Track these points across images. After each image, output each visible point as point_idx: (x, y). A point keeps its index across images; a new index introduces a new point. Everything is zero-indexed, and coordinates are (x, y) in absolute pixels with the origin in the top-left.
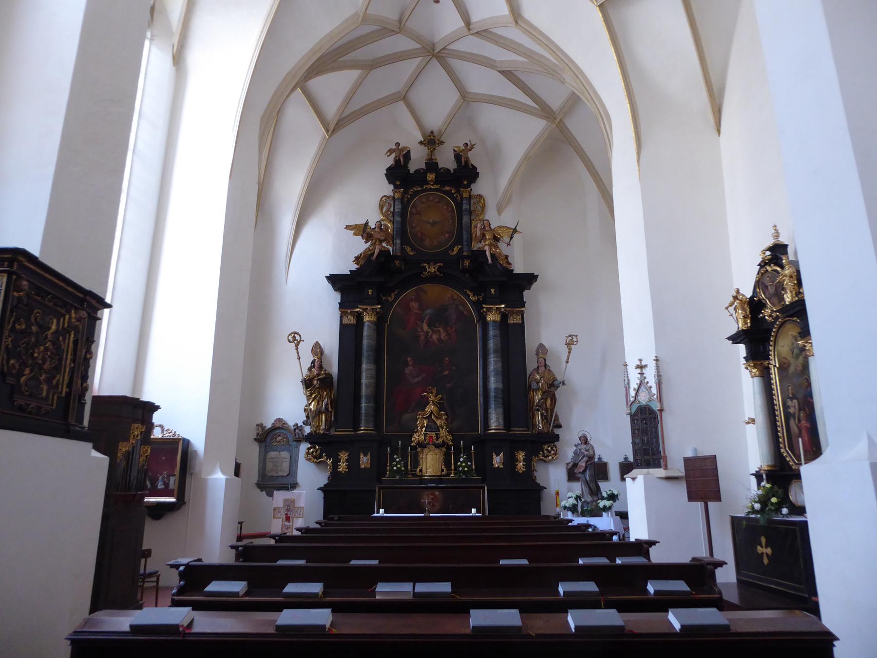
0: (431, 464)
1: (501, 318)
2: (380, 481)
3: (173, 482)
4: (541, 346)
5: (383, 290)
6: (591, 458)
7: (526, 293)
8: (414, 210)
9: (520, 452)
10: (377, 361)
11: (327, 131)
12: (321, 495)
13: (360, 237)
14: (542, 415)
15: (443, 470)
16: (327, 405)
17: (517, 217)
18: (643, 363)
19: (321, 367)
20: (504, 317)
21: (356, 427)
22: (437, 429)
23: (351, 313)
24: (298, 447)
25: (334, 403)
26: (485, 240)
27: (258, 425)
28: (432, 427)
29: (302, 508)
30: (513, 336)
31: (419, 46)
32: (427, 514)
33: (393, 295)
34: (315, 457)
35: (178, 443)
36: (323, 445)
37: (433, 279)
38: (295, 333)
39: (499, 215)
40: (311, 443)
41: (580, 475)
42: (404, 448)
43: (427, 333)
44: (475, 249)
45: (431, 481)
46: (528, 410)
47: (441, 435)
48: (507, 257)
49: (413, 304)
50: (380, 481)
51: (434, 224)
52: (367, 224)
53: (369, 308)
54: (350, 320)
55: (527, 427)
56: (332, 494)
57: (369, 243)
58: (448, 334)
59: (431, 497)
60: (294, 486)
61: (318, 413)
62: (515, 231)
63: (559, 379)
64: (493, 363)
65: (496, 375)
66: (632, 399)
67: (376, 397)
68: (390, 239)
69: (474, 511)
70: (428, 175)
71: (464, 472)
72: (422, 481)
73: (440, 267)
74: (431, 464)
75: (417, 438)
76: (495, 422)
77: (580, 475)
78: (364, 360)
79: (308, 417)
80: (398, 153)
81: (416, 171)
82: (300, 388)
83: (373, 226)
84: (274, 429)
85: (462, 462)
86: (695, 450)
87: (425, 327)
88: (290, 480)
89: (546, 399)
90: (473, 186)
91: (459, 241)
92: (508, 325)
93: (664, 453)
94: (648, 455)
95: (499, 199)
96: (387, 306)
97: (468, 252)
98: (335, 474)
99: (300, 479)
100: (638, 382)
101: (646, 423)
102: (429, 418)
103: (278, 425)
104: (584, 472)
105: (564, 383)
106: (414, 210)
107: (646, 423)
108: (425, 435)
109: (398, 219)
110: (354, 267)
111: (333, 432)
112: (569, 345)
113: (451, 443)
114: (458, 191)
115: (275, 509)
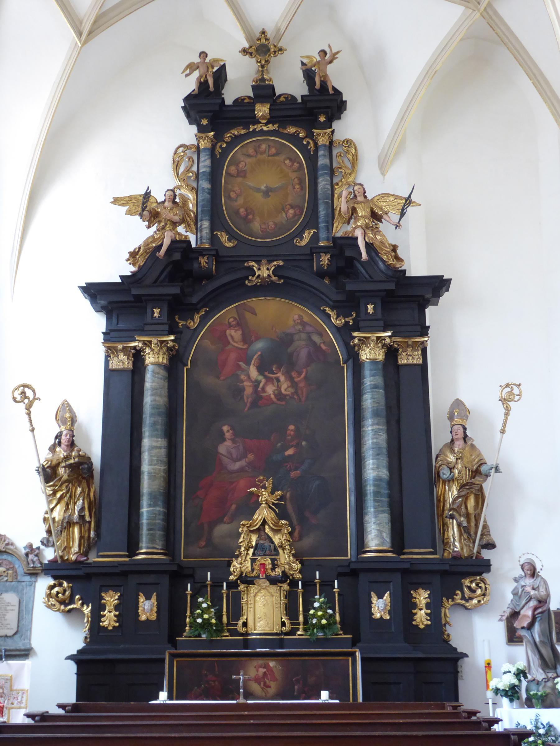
0: (263, 611)
1: (387, 355)
2: (173, 643)
4: (458, 403)
5: (178, 308)
6: (543, 602)
7: (430, 311)
11: (79, 34)
12: (72, 667)
13: (138, 218)
14: (459, 525)
15: (283, 624)
16: (82, 509)
19: (72, 445)
20: (392, 353)
21: (132, 547)
22: (274, 552)
23: (124, 349)
24: (32, 585)
25: (96, 506)
26: (357, 219)
28: (264, 548)
29: (24, 691)
30: (407, 388)
32: (242, 700)
33: (197, 317)
34: (62, 602)
36: (77, 580)
37: (266, 289)
38: (25, 386)
39: (383, 174)
40: (55, 577)
41: (523, 633)
42: (216, 585)
43: (258, 382)
44: (339, 235)
45: (264, 643)
46: (434, 514)
47: (283, 561)
48: (394, 248)
49: (233, 332)
50: (173, 643)
51: (267, 193)
52: (147, 195)
53: (154, 340)
54: (122, 362)
55: (434, 546)
56: (90, 666)
57: (154, 228)
58: (294, 384)
59: (262, 670)
60: (25, 653)
61: (68, 524)
62: (408, 201)
64: (374, 434)
65: (377, 455)
67: (169, 496)
68: (194, 223)
69: (325, 695)
70: (258, 107)
71: (322, 628)
72: (246, 644)
73: (278, 267)
74: (263, 611)
75: (237, 567)
76: (376, 536)
77: (523, 633)
78: (146, 431)
79: (49, 532)
80: (203, 69)
81: (236, 101)
82: (37, 481)
83: (160, 199)
85: (316, 609)
87: (254, 373)
88: (20, 644)
89: (466, 498)
90: (336, 125)
91: (311, 220)
92: (398, 367)
96: (184, 338)
97: (328, 240)
98: (96, 631)
99: (35, 643)
102: (260, 530)
104: (530, 627)
105: (497, 470)
106: (233, 170)
108: (253, 561)
109: (205, 185)
110: (128, 269)
111: (93, 558)
112: (505, 401)
113: (298, 576)
114: (310, 135)
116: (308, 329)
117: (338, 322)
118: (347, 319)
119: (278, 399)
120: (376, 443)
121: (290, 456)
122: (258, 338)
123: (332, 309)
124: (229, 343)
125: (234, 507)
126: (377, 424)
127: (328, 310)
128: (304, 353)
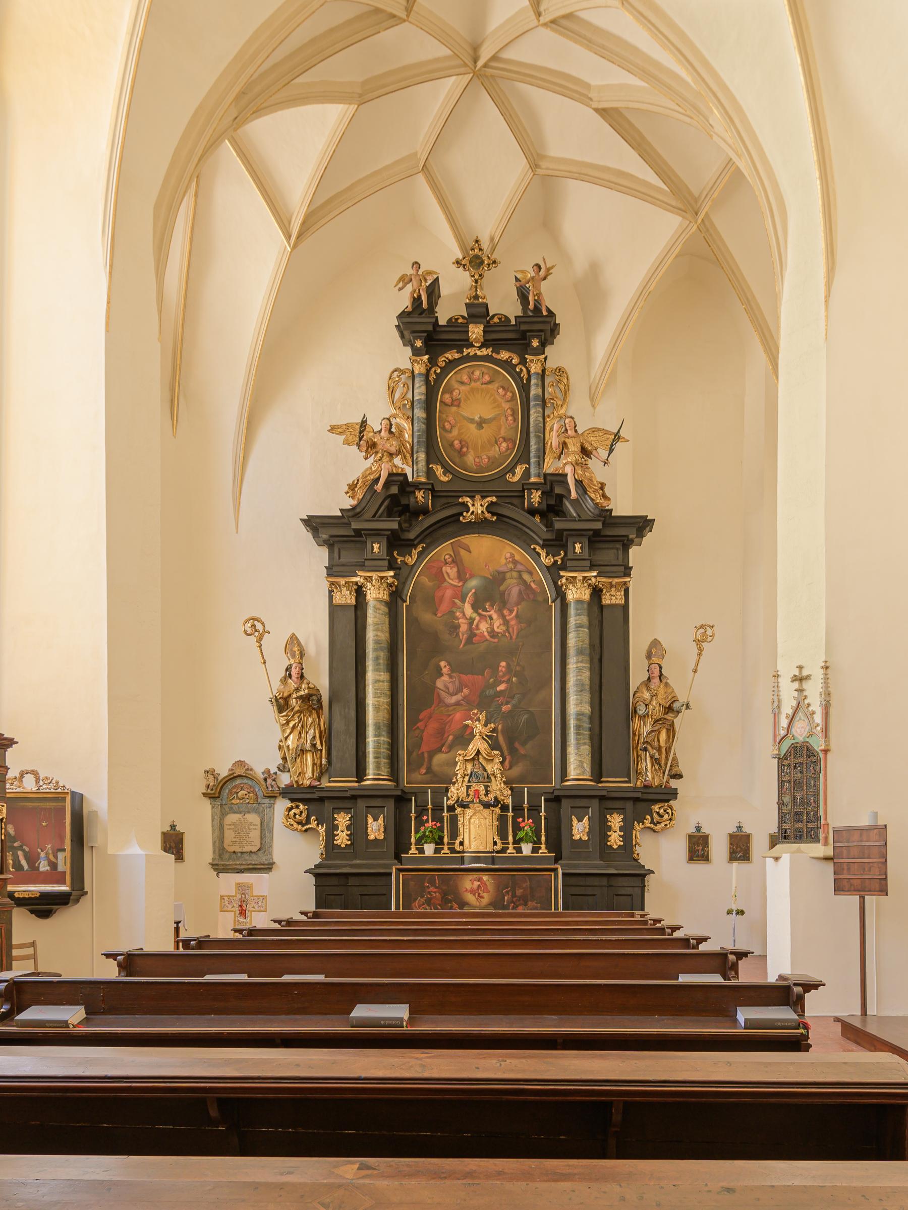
0: (477, 832)
1: (592, 594)
3: (64, 862)
4: (655, 643)
5: (397, 543)
7: (633, 551)
8: (447, 397)
9: (615, 816)
10: (393, 667)
11: (288, 237)
12: (312, 879)
14: (652, 757)
15: (495, 843)
17: (614, 411)
18: (805, 673)
20: (597, 593)
24: (271, 807)
25: (327, 736)
27: (207, 772)
30: (608, 627)
31: (446, 52)
33: (415, 553)
34: (300, 823)
35: (64, 799)
36: (313, 802)
37: (480, 526)
38: (254, 619)
40: (292, 800)
48: (602, 486)
50: (398, 858)
51: (481, 424)
52: (364, 424)
53: (375, 575)
55: (629, 776)
57: (371, 460)
58: (506, 623)
59: (477, 883)
62: (617, 437)
63: (682, 699)
65: (580, 691)
66: (783, 733)
70: (471, 327)
74: (477, 832)
75: (456, 791)
76: (578, 767)
81: (450, 320)
84: (232, 778)
86: (875, 815)
87: (468, 610)
90: (548, 350)
91: (523, 456)
92: (601, 607)
93: (826, 819)
94: (800, 821)
95: (597, 378)
98: (330, 847)
99: (277, 856)
100: (794, 703)
101: (801, 769)
103: (239, 772)
106: (447, 397)
107: (801, 769)
108: (468, 787)
109: (420, 413)
110: (349, 503)
111: (325, 783)
114: (523, 362)
115: (222, 897)
116: (519, 567)
117: (547, 561)
118: (556, 558)
119: (491, 637)
120: (580, 680)
121: (501, 691)
122: (472, 576)
123: (542, 547)
124: (445, 580)
125: (451, 738)
126: (581, 662)
127: (538, 549)
128: (515, 591)
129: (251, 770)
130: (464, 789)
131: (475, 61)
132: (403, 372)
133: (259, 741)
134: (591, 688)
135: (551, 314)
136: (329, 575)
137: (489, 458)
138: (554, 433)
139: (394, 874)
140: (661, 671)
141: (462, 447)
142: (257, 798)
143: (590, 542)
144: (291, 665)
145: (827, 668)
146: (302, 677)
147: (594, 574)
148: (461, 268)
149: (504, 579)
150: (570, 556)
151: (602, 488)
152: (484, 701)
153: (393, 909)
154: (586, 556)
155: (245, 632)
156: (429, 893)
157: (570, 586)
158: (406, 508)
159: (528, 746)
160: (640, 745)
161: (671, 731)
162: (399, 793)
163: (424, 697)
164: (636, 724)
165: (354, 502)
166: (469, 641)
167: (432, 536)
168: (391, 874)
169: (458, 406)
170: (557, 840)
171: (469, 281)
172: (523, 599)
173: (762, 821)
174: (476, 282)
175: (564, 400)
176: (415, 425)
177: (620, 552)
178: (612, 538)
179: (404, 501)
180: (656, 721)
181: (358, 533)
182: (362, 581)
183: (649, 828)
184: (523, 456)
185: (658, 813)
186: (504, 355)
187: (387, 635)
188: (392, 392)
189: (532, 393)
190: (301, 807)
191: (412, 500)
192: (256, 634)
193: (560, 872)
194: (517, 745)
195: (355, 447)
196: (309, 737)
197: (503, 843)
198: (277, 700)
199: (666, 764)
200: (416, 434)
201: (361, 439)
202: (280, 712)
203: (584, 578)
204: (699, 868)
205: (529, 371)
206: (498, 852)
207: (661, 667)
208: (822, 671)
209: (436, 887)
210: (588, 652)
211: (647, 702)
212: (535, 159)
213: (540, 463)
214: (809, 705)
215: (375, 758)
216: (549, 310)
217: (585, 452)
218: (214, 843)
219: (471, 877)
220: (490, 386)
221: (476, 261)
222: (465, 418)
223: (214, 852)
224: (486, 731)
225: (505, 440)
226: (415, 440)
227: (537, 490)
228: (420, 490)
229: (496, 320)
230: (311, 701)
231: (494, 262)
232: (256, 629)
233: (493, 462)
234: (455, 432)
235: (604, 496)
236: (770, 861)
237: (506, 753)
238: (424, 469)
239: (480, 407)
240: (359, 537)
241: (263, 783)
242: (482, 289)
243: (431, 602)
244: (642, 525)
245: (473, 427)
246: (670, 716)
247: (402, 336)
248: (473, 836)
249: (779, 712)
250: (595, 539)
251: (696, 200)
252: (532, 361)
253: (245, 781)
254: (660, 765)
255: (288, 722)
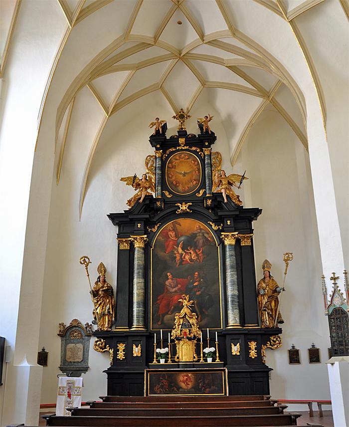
0: (185, 353)
1: (236, 242)
4: (266, 261)
5: (149, 223)
9: (253, 342)
10: (146, 276)
12: (106, 375)
14: (268, 314)
15: (194, 358)
18: (336, 276)
20: (238, 241)
24: (88, 340)
25: (115, 307)
27: (60, 324)
30: (245, 256)
34: (101, 348)
36: (108, 339)
37: (185, 215)
38: (85, 257)
40: (98, 338)
48: (238, 197)
51: (184, 175)
52: (135, 177)
55: (258, 323)
57: (138, 190)
58: (197, 255)
59: (186, 377)
62: (243, 177)
63: (281, 286)
65: (233, 285)
66: (329, 303)
74: (185, 353)
75: (175, 333)
76: (233, 320)
81: (171, 137)
84: (71, 327)
87: (180, 250)
90: (212, 146)
91: (203, 186)
92: (241, 247)
94: (342, 345)
98: (115, 359)
100: (333, 290)
103: (74, 324)
108: (181, 331)
109: (158, 172)
110: (127, 208)
114: (202, 151)
116: (203, 231)
117: (216, 228)
121: (196, 285)
122: (181, 236)
125: (173, 307)
127: (211, 223)
128: (201, 241)
129: (80, 323)
130: (179, 332)
131: (180, 55)
132: (152, 157)
133: (84, 310)
134: (238, 283)
135: (213, 133)
136: (118, 237)
137: (188, 188)
138: (216, 177)
139: (145, 373)
140: (270, 274)
141: (177, 184)
142: (82, 336)
143: (234, 220)
144: (100, 276)
145: (346, 273)
146: (105, 281)
147: (237, 233)
148: (176, 119)
149: (196, 236)
150: (225, 226)
151: (238, 198)
152: (188, 290)
153: (145, 396)
154: (233, 226)
155: (81, 263)
156: (162, 383)
157: (226, 239)
158: (153, 209)
159: (209, 311)
160: (262, 308)
161: (277, 302)
162: (148, 334)
163: (160, 289)
164: (260, 298)
165: (130, 208)
166: (181, 263)
167: (164, 220)
168: (144, 373)
169: (175, 168)
170: (224, 353)
171: (179, 123)
172: (205, 245)
173: (324, 343)
174: (182, 123)
175: (220, 164)
176: (157, 176)
177: (248, 224)
178: (244, 218)
179: (152, 206)
180: (269, 297)
181: (131, 219)
182: (133, 239)
183: (269, 347)
184: (203, 186)
185: (273, 341)
186: (194, 149)
187: (144, 262)
188: (147, 164)
189: (206, 162)
190: (102, 340)
191: (155, 205)
192: (86, 263)
193: (227, 371)
194: (204, 310)
195: (131, 186)
196: (107, 308)
197: (198, 357)
198: (93, 292)
199: (275, 317)
200: (157, 180)
201: (134, 183)
202: (94, 297)
203: (232, 235)
204: (295, 366)
205: (204, 154)
206: (196, 362)
207: (270, 272)
208: (344, 275)
209: (166, 380)
210: (235, 267)
211: (264, 288)
212: (204, 83)
213: (210, 189)
214: (340, 290)
215: (137, 318)
216: (211, 131)
217: (230, 184)
218: (61, 357)
219: (183, 375)
220: (188, 160)
221: (181, 116)
222: (178, 173)
223: (61, 362)
224: (189, 304)
225: (195, 180)
226: (157, 182)
227: (210, 199)
228: (158, 201)
229: (190, 136)
230: (109, 292)
231: (189, 116)
232: (85, 261)
233: (190, 189)
234: (174, 178)
235: (239, 201)
236: (329, 365)
237: (199, 314)
238: (160, 193)
239: (184, 169)
240: (133, 222)
241: (85, 329)
242: (184, 125)
243: (163, 247)
244: (256, 212)
245: (181, 175)
246: (275, 294)
247: (151, 144)
248: (183, 354)
249: (326, 294)
250: (235, 219)
251: (268, 93)
252: (205, 150)
253: (77, 328)
254: (273, 317)
255: (98, 302)
